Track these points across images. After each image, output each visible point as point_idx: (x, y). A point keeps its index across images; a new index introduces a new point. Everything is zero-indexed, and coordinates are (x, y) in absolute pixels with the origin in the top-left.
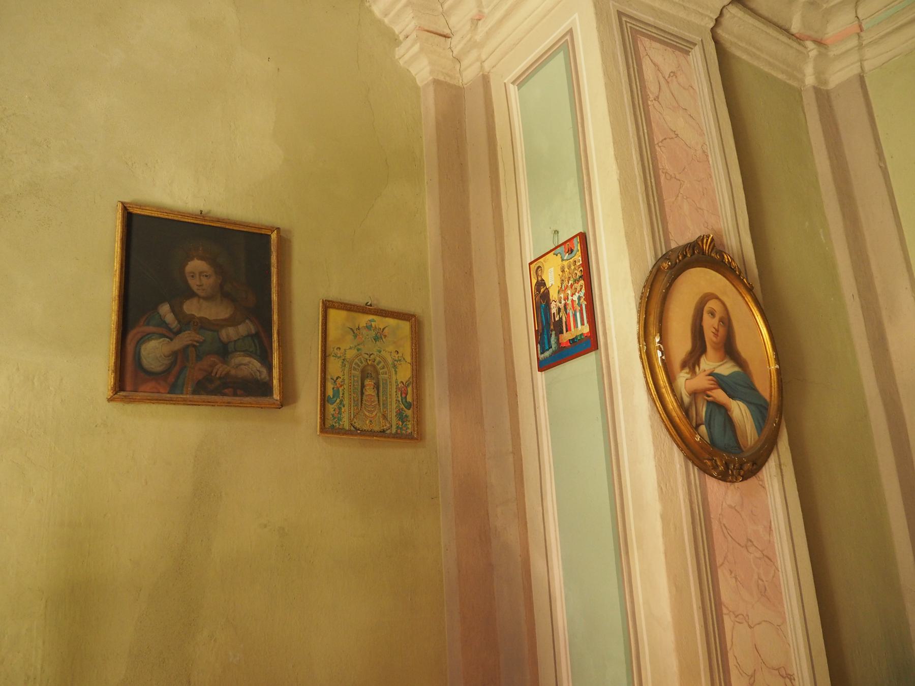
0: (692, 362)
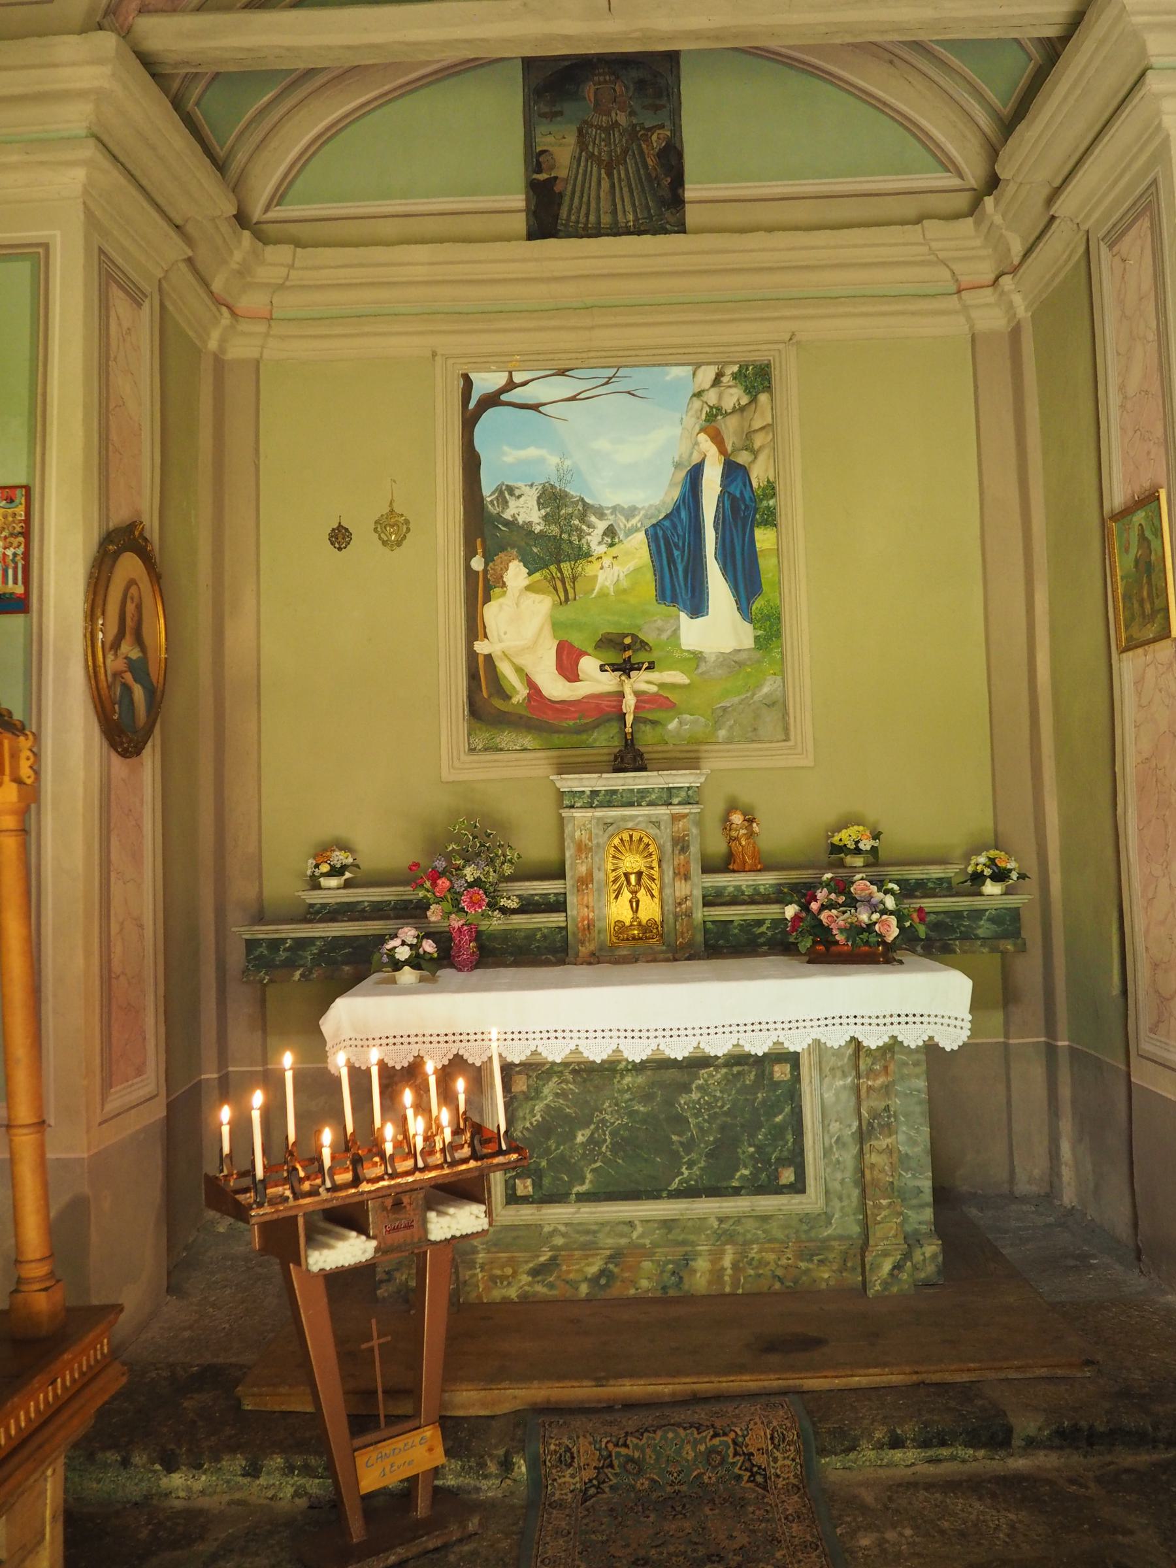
0: (116, 645)
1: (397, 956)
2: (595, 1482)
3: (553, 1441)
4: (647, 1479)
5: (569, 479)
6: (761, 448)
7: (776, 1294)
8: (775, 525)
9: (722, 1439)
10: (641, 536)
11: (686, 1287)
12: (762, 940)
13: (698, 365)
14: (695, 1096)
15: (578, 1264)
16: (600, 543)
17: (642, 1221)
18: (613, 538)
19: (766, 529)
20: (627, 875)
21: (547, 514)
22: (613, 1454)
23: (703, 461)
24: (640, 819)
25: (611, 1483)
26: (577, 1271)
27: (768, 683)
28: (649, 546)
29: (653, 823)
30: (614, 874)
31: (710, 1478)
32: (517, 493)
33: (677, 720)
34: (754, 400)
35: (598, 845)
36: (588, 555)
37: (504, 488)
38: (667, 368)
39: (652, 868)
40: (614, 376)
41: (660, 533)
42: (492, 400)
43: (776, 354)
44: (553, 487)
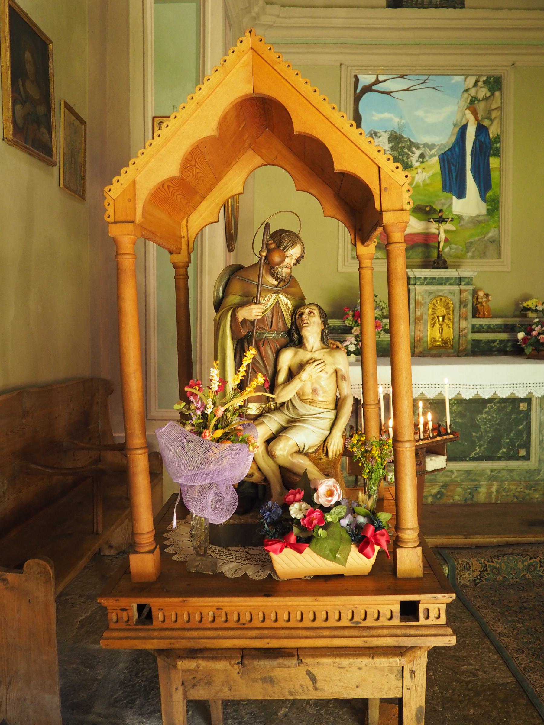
1: (350, 349)
2: (479, 577)
3: (460, 560)
4: (502, 576)
5: (403, 129)
6: (495, 118)
7: (515, 503)
8: (499, 156)
9: (534, 560)
10: (436, 159)
11: (475, 499)
12: (494, 349)
13: (467, 76)
14: (484, 416)
15: (428, 488)
16: (417, 161)
17: (456, 470)
18: (423, 159)
19: (495, 158)
20: (438, 317)
21: (393, 146)
22: (488, 566)
23: (467, 124)
24: (445, 291)
25: (486, 578)
26: (427, 491)
27: (492, 232)
28: (440, 164)
29: (451, 293)
30: (432, 316)
31: (529, 576)
32: (379, 135)
33: (449, 247)
34: (493, 94)
35: (425, 303)
36: (411, 167)
37: (372, 132)
38: (452, 77)
39: (449, 314)
40: (427, 80)
41: (446, 158)
42: (368, 89)
43: (505, 72)
44: (396, 133)
